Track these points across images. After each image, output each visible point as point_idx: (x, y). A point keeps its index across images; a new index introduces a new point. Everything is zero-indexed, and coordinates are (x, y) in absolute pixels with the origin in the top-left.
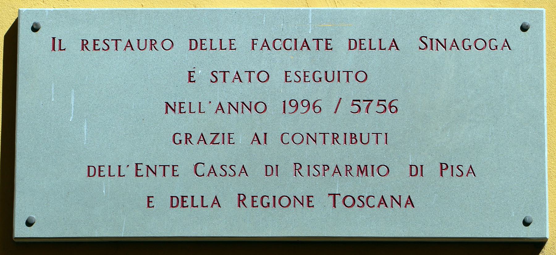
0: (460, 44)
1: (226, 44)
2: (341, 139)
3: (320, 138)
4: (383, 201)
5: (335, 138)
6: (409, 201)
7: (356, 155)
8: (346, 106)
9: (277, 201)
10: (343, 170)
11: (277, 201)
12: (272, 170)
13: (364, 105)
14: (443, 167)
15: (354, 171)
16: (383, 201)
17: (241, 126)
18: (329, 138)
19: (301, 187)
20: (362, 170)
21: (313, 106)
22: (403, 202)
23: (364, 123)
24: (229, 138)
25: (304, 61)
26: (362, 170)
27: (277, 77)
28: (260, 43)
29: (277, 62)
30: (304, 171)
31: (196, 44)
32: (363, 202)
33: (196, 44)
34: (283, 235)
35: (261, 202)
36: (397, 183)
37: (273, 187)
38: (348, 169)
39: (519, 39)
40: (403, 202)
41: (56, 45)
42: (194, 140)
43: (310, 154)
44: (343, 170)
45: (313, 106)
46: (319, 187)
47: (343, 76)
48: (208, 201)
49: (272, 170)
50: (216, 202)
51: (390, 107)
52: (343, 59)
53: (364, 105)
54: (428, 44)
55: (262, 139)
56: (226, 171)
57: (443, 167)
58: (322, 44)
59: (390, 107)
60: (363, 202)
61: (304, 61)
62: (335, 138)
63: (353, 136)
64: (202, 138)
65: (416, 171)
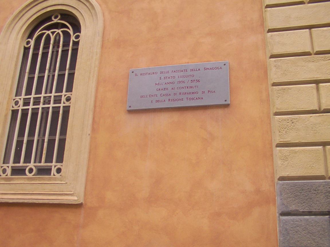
0: (212, 69)
1: (167, 72)
2: (189, 88)
3: (185, 88)
4: (197, 98)
5: (188, 87)
6: (202, 98)
7: (191, 90)
8: (190, 82)
9: (176, 100)
10: (189, 93)
11: (176, 100)
12: (175, 94)
13: (193, 81)
14: (209, 91)
15: (191, 93)
16: (197, 98)
17: (169, 86)
18: (186, 87)
19: (181, 97)
20: (193, 93)
21: (184, 82)
22: (201, 98)
23: (193, 84)
24: (167, 89)
25: (182, 74)
26: (193, 93)
27: (177, 77)
28: (173, 72)
29: (176, 75)
30: (181, 94)
31: (161, 73)
32: (193, 99)
33: (161, 73)
34: (77, 64)
35: (174, 100)
36: (199, 95)
37: (176, 97)
38: (190, 93)
39: (223, 67)
40: (201, 98)
41: (136, 75)
42: (161, 90)
43: (183, 91)
44: (189, 93)
45: (184, 82)
46: (184, 97)
47: (189, 76)
48: (163, 101)
49: (175, 94)
50: (164, 101)
51: (199, 81)
52: (189, 73)
53: (193, 81)
54: (205, 69)
55: (173, 89)
56: (167, 95)
57: (209, 91)
58: (185, 70)
59: (199, 81)
60: (193, 99)
61: (182, 74)
62: (188, 87)
63: (191, 87)
64: (162, 89)
65: (203, 92)
